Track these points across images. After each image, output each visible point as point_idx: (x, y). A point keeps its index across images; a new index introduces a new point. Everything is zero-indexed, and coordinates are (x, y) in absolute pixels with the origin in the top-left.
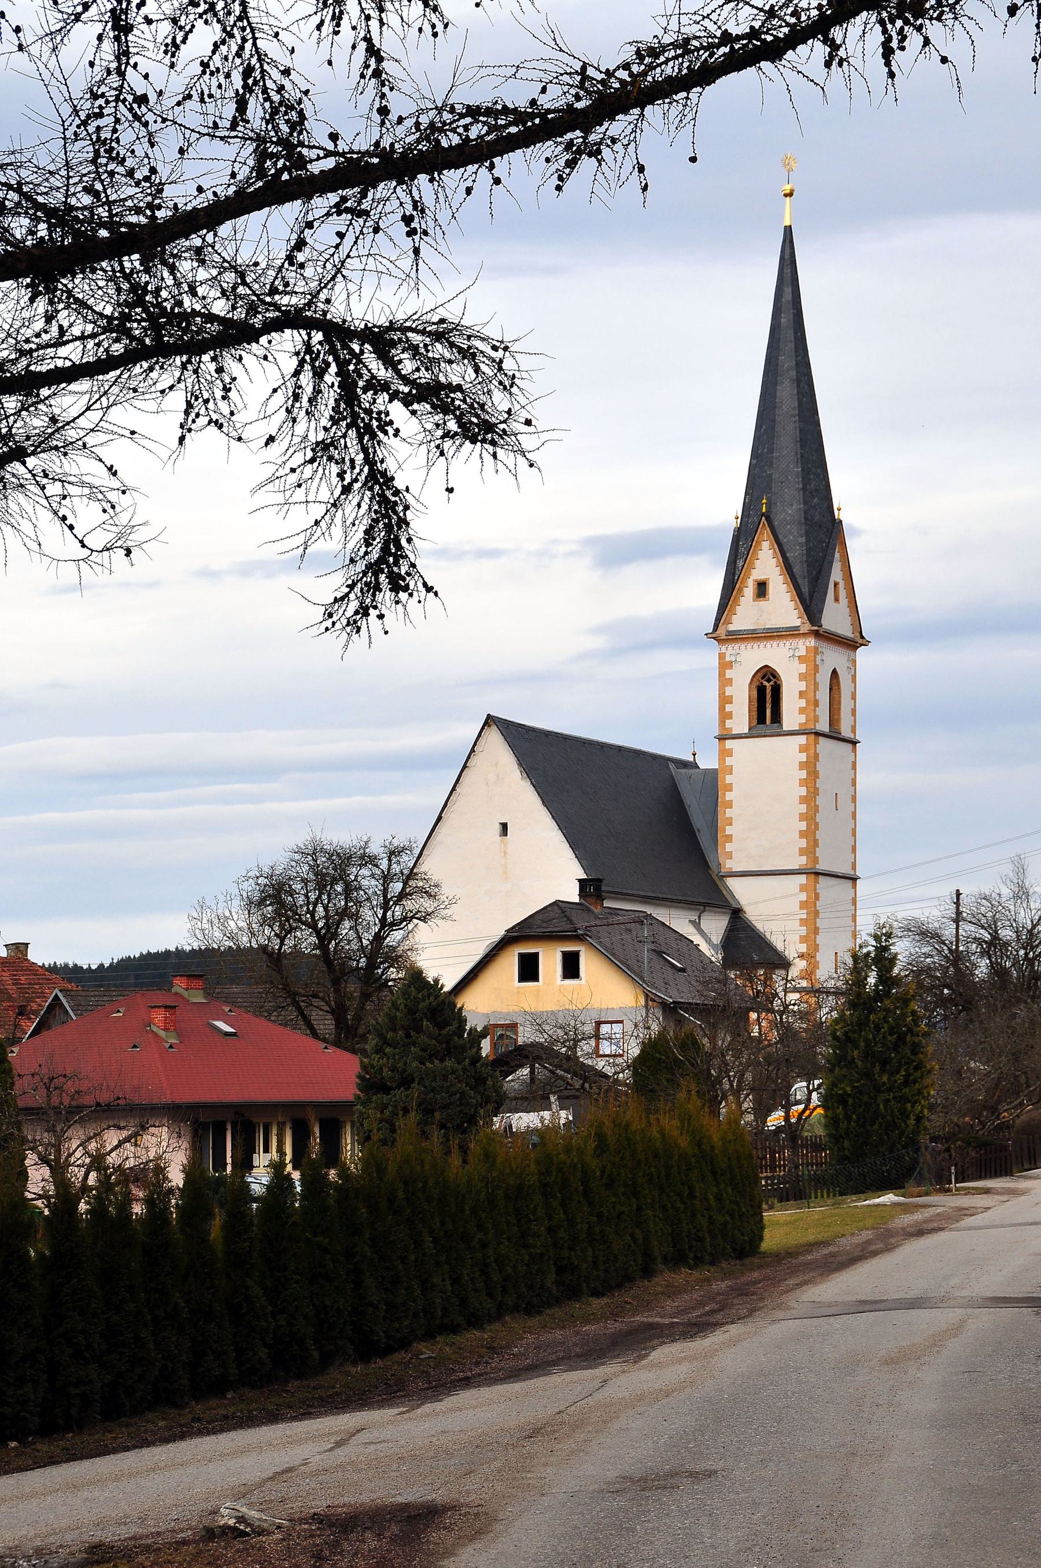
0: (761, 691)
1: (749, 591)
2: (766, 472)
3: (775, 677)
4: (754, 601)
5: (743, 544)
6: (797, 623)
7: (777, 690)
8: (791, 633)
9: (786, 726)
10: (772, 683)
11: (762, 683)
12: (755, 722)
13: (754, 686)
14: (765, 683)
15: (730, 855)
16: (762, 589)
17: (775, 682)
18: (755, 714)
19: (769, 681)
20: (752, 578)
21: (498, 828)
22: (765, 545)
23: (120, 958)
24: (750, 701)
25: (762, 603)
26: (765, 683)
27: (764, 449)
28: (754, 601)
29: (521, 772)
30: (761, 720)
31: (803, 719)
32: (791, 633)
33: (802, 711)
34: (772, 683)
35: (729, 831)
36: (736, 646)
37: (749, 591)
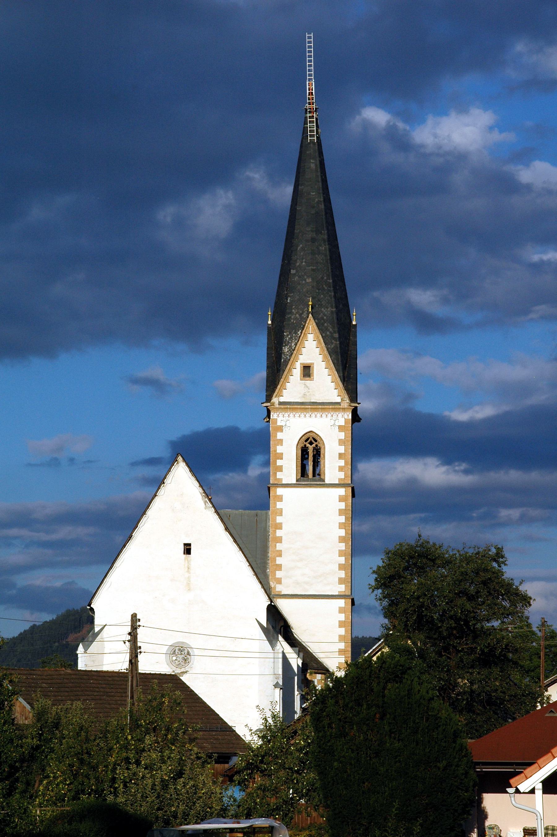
0: (304, 452)
1: (297, 371)
2: (305, 280)
3: (316, 441)
4: (301, 380)
5: (288, 335)
6: (338, 400)
7: (318, 453)
8: (332, 406)
9: (328, 480)
10: (314, 445)
11: (305, 445)
12: (300, 475)
13: (300, 447)
14: (308, 445)
15: (279, 581)
16: (307, 371)
17: (317, 446)
18: (300, 471)
19: (311, 443)
20: (299, 362)
21: (182, 548)
22: (311, 337)
23: (357, 636)
24: (297, 459)
25: (308, 382)
26: (308, 445)
27: (302, 262)
28: (301, 380)
29: (205, 502)
30: (303, 472)
31: (342, 475)
32: (332, 406)
33: (341, 469)
34: (314, 445)
35: (279, 561)
36: (286, 415)
37: (297, 371)
